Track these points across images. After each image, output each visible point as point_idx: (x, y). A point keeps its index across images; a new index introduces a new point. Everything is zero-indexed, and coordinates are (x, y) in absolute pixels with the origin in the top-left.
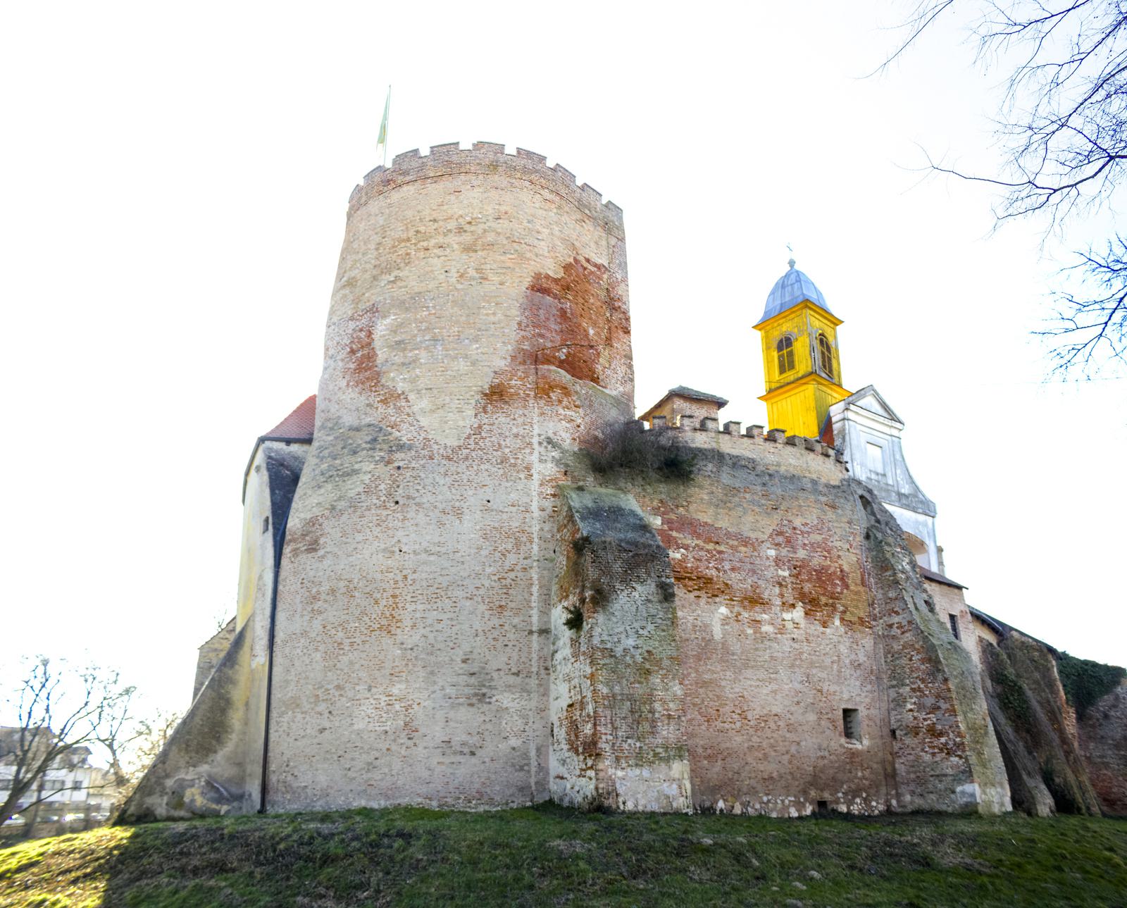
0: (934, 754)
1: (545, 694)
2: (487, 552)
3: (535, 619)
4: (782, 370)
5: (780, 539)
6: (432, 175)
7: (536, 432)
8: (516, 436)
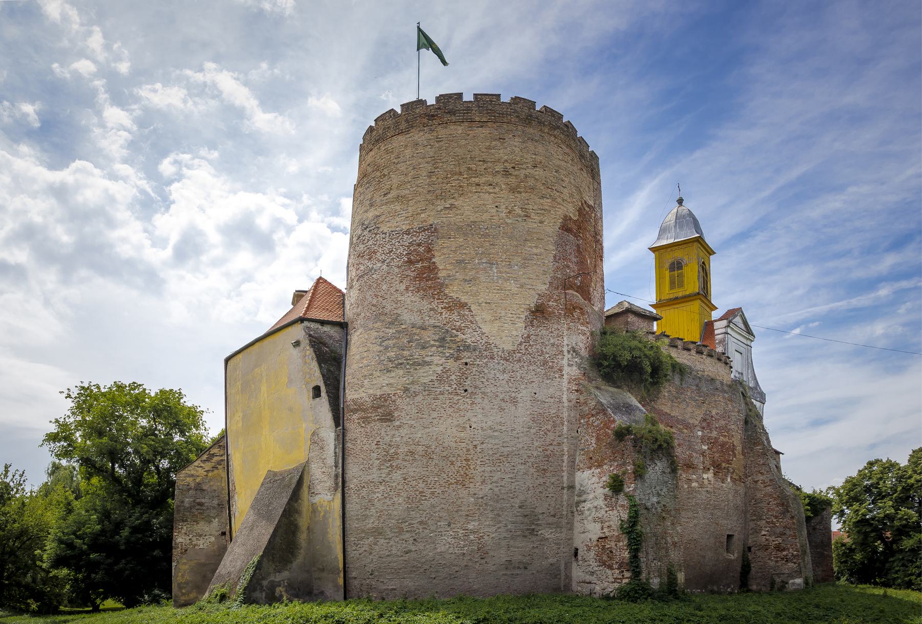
0: (777, 562)
1: (571, 529)
2: (534, 431)
3: (565, 478)
4: (672, 285)
5: (704, 424)
6: (477, 119)
7: (566, 342)
8: (553, 345)
